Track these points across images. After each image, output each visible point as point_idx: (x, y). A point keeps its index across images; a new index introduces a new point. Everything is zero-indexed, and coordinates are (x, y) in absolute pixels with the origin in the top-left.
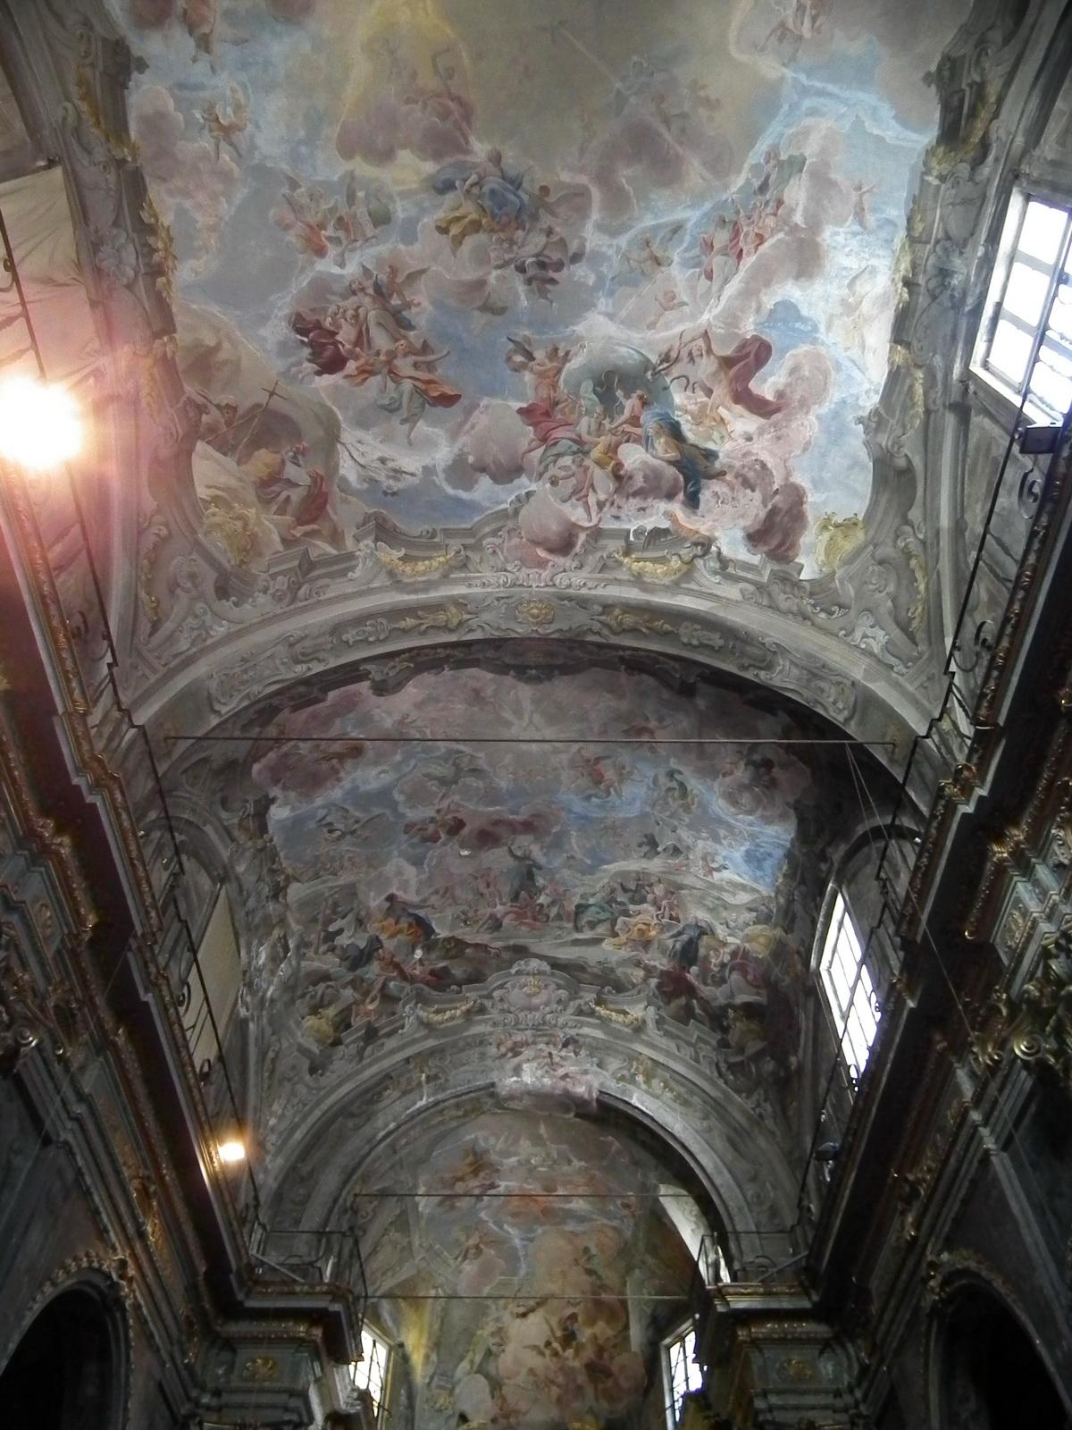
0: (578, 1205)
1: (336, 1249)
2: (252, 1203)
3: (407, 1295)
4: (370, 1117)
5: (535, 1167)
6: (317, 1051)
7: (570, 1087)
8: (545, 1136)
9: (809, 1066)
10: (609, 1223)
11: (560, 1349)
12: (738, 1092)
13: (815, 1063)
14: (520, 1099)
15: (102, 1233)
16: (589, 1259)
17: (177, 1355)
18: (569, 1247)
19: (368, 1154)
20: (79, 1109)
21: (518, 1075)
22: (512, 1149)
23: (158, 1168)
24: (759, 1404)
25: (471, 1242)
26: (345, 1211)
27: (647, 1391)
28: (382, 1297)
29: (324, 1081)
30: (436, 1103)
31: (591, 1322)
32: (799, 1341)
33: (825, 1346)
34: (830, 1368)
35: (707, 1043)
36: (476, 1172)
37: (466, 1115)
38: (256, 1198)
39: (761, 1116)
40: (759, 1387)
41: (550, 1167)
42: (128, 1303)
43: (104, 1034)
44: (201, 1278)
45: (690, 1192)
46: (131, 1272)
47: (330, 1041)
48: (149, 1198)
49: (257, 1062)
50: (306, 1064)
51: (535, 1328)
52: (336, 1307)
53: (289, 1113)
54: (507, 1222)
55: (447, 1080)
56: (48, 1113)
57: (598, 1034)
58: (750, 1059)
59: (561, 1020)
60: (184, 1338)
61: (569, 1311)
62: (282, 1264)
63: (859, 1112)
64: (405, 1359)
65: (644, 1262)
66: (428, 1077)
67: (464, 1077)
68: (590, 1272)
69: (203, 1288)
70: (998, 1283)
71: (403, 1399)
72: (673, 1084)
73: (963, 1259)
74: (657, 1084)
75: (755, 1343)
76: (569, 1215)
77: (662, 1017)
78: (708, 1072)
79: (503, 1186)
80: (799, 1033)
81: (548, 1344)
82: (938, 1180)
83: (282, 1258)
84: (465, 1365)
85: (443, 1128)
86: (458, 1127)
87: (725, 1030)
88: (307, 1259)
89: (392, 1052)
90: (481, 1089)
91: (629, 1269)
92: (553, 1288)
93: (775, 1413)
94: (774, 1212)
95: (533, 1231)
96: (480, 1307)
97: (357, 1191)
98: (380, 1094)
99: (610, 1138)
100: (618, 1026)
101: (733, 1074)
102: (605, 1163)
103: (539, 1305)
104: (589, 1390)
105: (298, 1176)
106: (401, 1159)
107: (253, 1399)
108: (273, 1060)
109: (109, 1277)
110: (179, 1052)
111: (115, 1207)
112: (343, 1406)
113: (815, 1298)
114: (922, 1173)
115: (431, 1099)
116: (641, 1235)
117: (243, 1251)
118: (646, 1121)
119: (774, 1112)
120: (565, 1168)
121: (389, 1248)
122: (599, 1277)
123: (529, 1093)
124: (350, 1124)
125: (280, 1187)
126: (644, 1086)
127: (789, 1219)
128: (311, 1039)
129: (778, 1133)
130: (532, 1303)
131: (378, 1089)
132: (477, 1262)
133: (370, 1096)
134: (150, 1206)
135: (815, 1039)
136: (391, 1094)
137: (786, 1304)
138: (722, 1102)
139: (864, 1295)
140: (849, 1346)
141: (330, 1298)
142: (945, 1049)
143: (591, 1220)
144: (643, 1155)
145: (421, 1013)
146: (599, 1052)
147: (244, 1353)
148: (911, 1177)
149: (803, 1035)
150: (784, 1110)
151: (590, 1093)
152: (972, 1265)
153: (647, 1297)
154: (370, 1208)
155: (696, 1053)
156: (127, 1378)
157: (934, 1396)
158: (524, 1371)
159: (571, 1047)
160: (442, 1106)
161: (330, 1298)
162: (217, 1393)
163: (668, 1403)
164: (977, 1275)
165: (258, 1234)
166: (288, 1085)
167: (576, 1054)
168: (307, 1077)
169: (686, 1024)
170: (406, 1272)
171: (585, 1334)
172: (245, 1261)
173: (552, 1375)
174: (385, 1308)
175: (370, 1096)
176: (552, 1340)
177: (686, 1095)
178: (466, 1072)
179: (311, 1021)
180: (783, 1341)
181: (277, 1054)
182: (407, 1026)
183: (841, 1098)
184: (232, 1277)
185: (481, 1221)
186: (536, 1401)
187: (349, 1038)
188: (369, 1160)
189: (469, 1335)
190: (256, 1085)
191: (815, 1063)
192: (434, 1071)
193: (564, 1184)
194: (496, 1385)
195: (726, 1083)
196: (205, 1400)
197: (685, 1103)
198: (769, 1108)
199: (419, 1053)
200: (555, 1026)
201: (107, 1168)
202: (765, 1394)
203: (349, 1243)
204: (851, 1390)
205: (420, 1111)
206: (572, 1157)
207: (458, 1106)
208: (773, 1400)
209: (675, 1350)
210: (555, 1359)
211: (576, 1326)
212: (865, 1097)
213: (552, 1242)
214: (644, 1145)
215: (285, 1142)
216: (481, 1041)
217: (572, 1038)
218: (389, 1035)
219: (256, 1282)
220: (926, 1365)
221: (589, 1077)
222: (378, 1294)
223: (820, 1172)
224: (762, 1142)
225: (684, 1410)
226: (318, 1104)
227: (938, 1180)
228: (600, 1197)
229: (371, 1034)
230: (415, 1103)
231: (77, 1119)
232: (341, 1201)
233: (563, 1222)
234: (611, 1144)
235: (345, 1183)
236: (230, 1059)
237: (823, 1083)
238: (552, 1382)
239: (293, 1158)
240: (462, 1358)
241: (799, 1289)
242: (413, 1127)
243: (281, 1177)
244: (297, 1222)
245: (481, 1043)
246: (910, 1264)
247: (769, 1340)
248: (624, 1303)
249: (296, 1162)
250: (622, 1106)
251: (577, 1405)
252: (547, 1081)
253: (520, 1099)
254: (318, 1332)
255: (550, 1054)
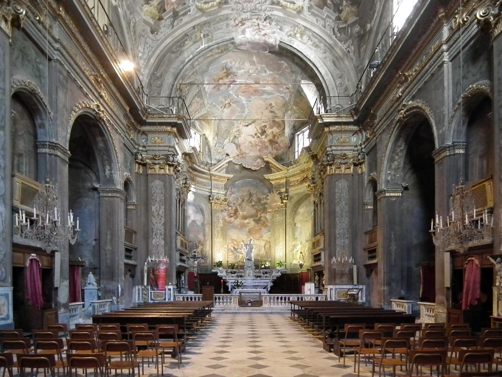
0: (269, 88)
1: (176, 104)
2: (140, 87)
3: (204, 119)
4: (181, 52)
5: (252, 74)
6: (152, 23)
7: (267, 40)
8: (256, 61)
9: (375, 29)
10: (280, 95)
11: (260, 136)
12: (341, 41)
13: (378, 27)
14: (245, 45)
15: (86, 95)
16: (271, 108)
17: (127, 136)
18: (264, 104)
19: (183, 68)
20: (57, 46)
21: (244, 34)
22: (242, 67)
23: (99, 72)
24: (328, 149)
25: (227, 102)
26: (178, 90)
27: (289, 147)
28: (196, 120)
29: (158, 37)
30: (209, 47)
31: (271, 127)
32: (346, 131)
33: (356, 132)
34: (355, 139)
35: (330, 18)
36: (227, 76)
37: (222, 52)
38: (141, 84)
39: (349, 52)
40: (329, 144)
41: (257, 74)
42: (105, 119)
43: (54, 10)
44: (128, 112)
45: (313, 82)
46: (102, 109)
47: (157, 18)
48: (100, 84)
49: (127, 28)
50: (149, 29)
51: (252, 129)
52: (180, 122)
53: (147, 51)
54: (240, 95)
55: (212, 37)
56: (46, 48)
57: (281, 14)
58: (348, 26)
59: (263, 7)
60: (128, 131)
61: (263, 125)
62: (157, 108)
63: (393, 48)
64: (206, 139)
65: (292, 108)
66: (204, 35)
67: (220, 35)
68: (271, 112)
69: (129, 115)
70: (427, 111)
71: (207, 150)
72: (312, 37)
73: (418, 103)
74: (305, 38)
75: (330, 132)
76: (264, 92)
77: (311, 5)
78: (329, 32)
79: (238, 81)
80: (374, 14)
81: (256, 134)
82: (417, 76)
83: (157, 106)
84: (227, 140)
85: (212, 58)
86: (219, 57)
87: (340, 12)
88: (166, 107)
89: (187, 23)
90: (227, 41)
91: (286, 111)
92: (257, 117)
93: (333, 151)
94: (346, 89)
95: (250, 98)
96: (231, 123)
97: (181, 83)
98: (184, 43)
99: (283, 62)
100: (290, 10)
101: (340, 33)
102: (280, 72)
103: (252, 122)
104: (270, 147)
105: (156, 76)
106: (196, 70)
107: (157, 148)
108: (134, 27)
109: (94, 110)
110: (91, 20)
111: (87, 85)
112: (188, 151)
113: (355, 118)
114: (411, 73)
115: (207, 45)
116: (292, 99)
117: (142, 104)
118: (299, 54)
119: (355, 50)
120: (264, 74)
121: (195, 104)
122: (275, 113)
123: (249, 42)
124: (173, 56)
125: (150, 80)
126: (300, 39)
127: (352, 92)
128: (149, 17)
129: (354, 59)
130: (250, 122)
131: (182, 41)
132: (229, 109)
133: (180, 43)
134: (101, 86)
135: (381, 18)
136: (189, 43)
137: (344, 120)
138: (333, 46)
139: (374, 116)
140: (364, 132)
141: (177, 119)
142: (443, 16)
143: (273, 94)
144: (296, 69)
145: (198, 4)
146: (280, 23)
147: (150, 136)
148: (407, 74)
149: (376, 14)
150: (359, 48)
151: (276, 42)
152: (420, 105)
153: (292, 119)
154: (186, 90)
155: (325, 23)
156: (113, 142)
157: (390, 145)
158: (247, 142)
159: (268, 21)
160: (211, 48)
161: (177, 119)
162: (144, 147)
163: (296, 150)
164: (421, 108)
165: (145, 98)
166: (143, 39)
167: (270, 24)
168: (151, 35)
169: (322, 8)
170: (203, 112)
171: (269, 131)
172: (143, 107)
173: (257, 143)
174: (197, 123)
175: (180, 43)
176: (257, 133)
177: (317, 41)
178: (220, 33)
179: (146, 8)
180: (340, 131)
181: (135, 23)
182: (192, 11)
183: (386, 41)
184: (140, 112)
185: (230, 94)
186: (251, 150)
187: (166, 16)
188: (183, 71)
189: (228, 132)
190: (129, 38)
191: (378, 27)
192: (207, 32)
193: (263, 80)
194: (238, 146)
195: (336, 37)
196: (141, 148)
197: (317, 46)
198: (353, 48)
199: (199, 24)
200: (261, 10)
201: (78, 70)
202: (331, 147)
203: (181, 101)
204: (361, 145)
205: (202, 50)
206: (266, 70)
207: (218, 48)
208: (333, 148)
209: (300, 136)
210: (258, 139)
211: (266, 129)
212: (398, 41)
213: (257, 102)
214: (297, 64)
215: (147, 63)
216: (227, 18)
217: (268, 16)
218: (184, 15)
219: (149, 114)
220: (390, 137)
221: (275, 35)
222: (194, 119)
223: (369, 73)
224: (347, 62)
225: (302, 152)
226: (158, 46)
227: (417, 76)
228: (277, 85)
229: (176, 15)
230: (199, 47)
231: (58, 50)
232: (175, 86)
233: (262, 94)
234: (284, 64)
235: (176, 79)
236: (114, 24)
237: (380, 36)
238: (257, 145)
239: (152, 70)
240: (226, 139)
241: (350, 115)
242: (200, 57)
243: (149, 78)
244: (159, 94)
245: (227, 19)
246: (396, 105)
247: (336, 131)
248: (284, 122)
249: (154, 71)
250: (289, 48)
251: (265, 151)
252: (257, 37)
253: (245, 45)
254: (175, 129)
255: (258, 24)
